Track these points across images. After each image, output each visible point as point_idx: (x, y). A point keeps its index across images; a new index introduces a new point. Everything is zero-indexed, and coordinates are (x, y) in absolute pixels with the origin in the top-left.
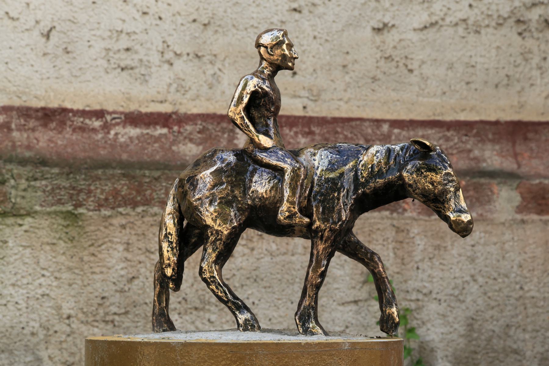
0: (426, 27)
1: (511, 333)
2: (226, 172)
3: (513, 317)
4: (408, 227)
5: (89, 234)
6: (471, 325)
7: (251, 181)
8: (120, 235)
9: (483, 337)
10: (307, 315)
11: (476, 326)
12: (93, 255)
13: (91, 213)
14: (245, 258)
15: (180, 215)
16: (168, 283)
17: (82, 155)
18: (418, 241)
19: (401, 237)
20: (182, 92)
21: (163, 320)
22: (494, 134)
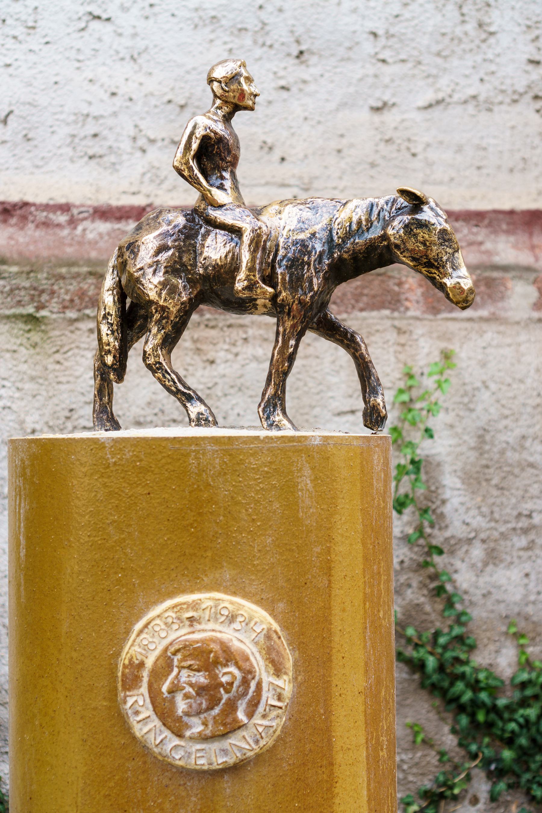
0: (430, 106)
1: (528, 444)
2: (173, 235)
3: (529, 426)
4: (411, 328)
5: (53, 339)
6: (482, 437)
7: (203, 246)
8: (88, 340)
9: (495, 450)
10: (274, 401)
11: (488, 438)
12: (58, 362)
13: (54, 316)
14: (228, 364)
15: (121, 294)
16: (110, 373)
17: (45, 253)
18: (422, 342)
19: (403, 339)
20: (158, 181)
21: (105, 417)
22: (508, 224)
